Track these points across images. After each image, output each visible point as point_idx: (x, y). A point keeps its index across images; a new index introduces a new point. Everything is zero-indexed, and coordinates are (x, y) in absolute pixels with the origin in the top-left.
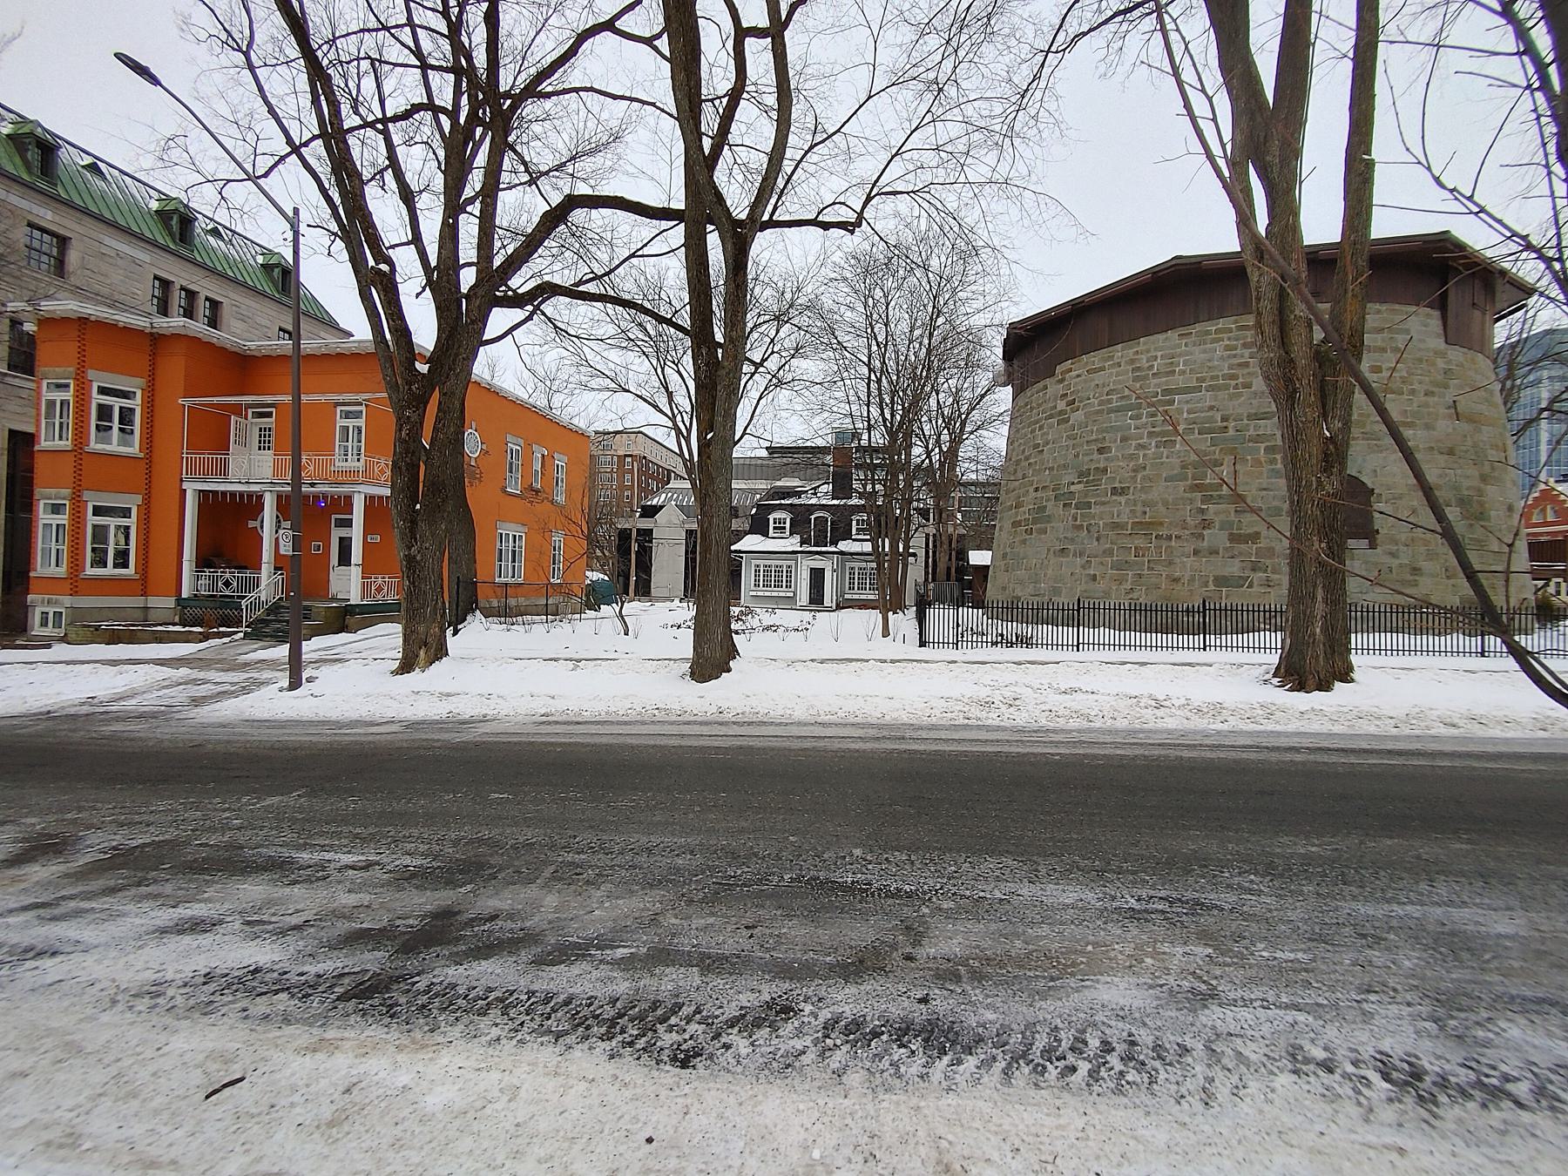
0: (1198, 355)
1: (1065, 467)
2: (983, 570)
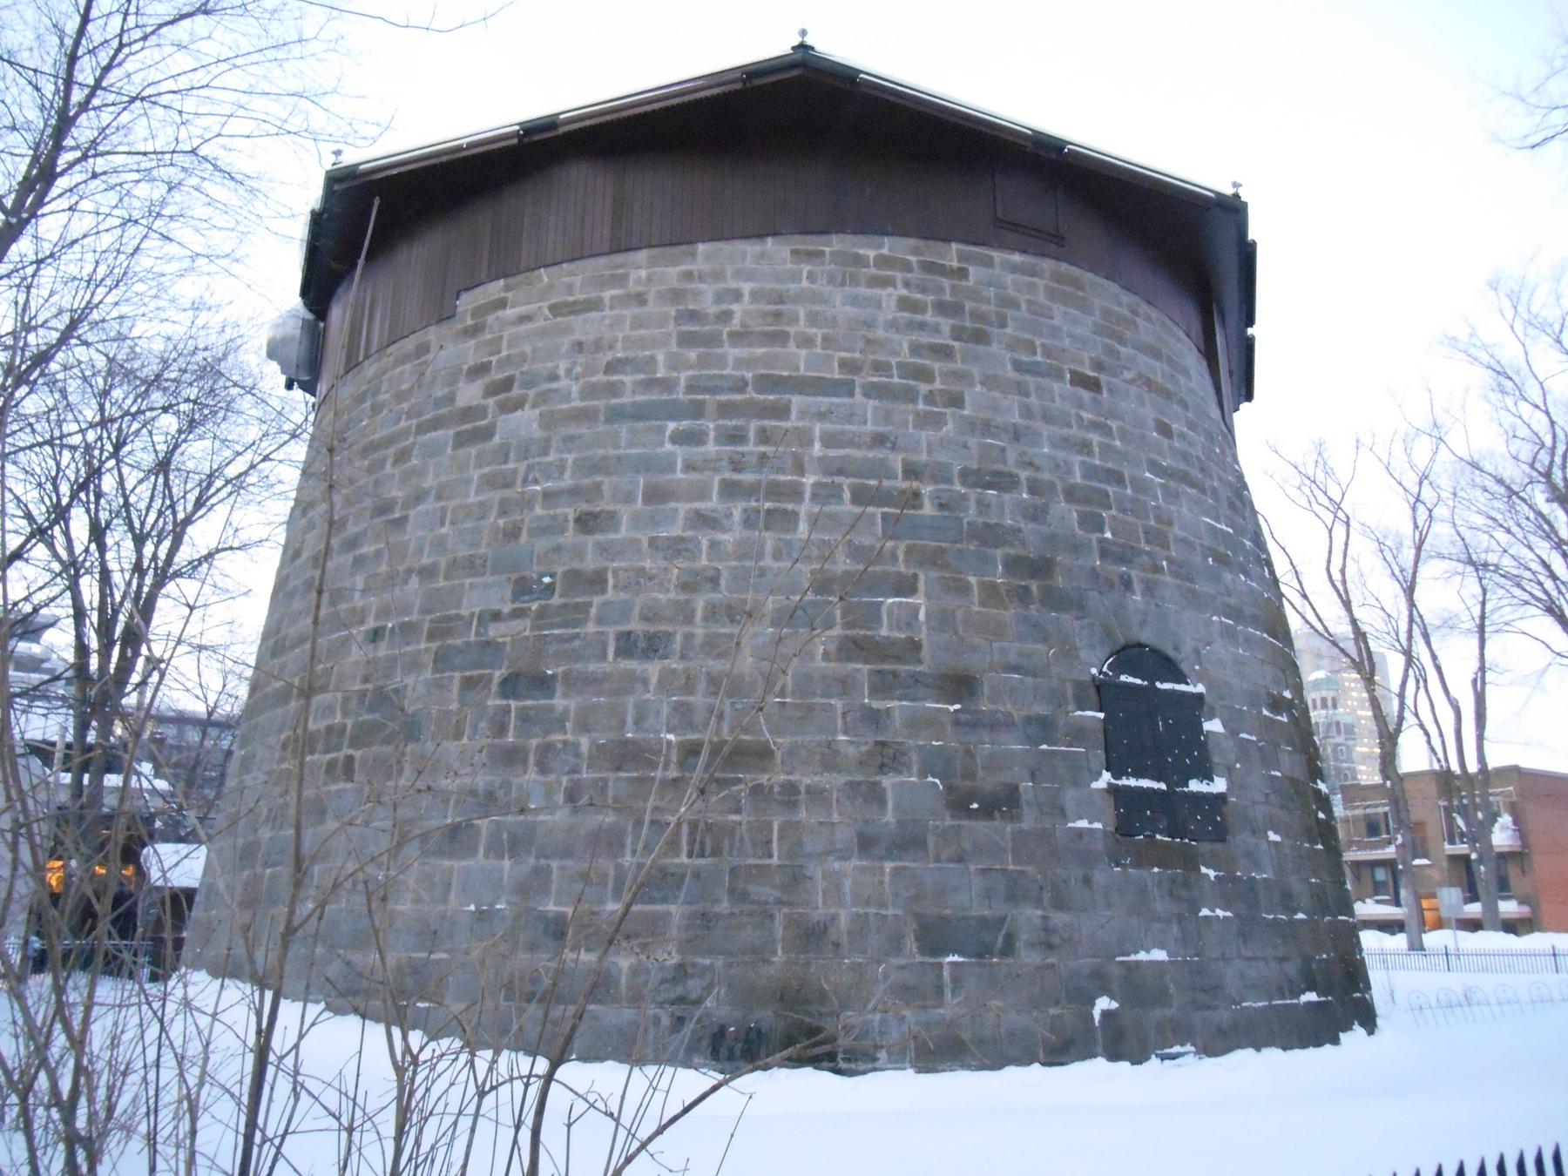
0: (840, 305)
1: (472, 566)
2: (181, 900)
